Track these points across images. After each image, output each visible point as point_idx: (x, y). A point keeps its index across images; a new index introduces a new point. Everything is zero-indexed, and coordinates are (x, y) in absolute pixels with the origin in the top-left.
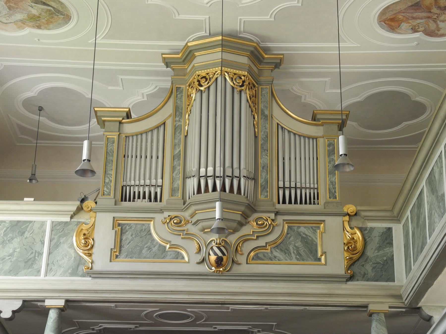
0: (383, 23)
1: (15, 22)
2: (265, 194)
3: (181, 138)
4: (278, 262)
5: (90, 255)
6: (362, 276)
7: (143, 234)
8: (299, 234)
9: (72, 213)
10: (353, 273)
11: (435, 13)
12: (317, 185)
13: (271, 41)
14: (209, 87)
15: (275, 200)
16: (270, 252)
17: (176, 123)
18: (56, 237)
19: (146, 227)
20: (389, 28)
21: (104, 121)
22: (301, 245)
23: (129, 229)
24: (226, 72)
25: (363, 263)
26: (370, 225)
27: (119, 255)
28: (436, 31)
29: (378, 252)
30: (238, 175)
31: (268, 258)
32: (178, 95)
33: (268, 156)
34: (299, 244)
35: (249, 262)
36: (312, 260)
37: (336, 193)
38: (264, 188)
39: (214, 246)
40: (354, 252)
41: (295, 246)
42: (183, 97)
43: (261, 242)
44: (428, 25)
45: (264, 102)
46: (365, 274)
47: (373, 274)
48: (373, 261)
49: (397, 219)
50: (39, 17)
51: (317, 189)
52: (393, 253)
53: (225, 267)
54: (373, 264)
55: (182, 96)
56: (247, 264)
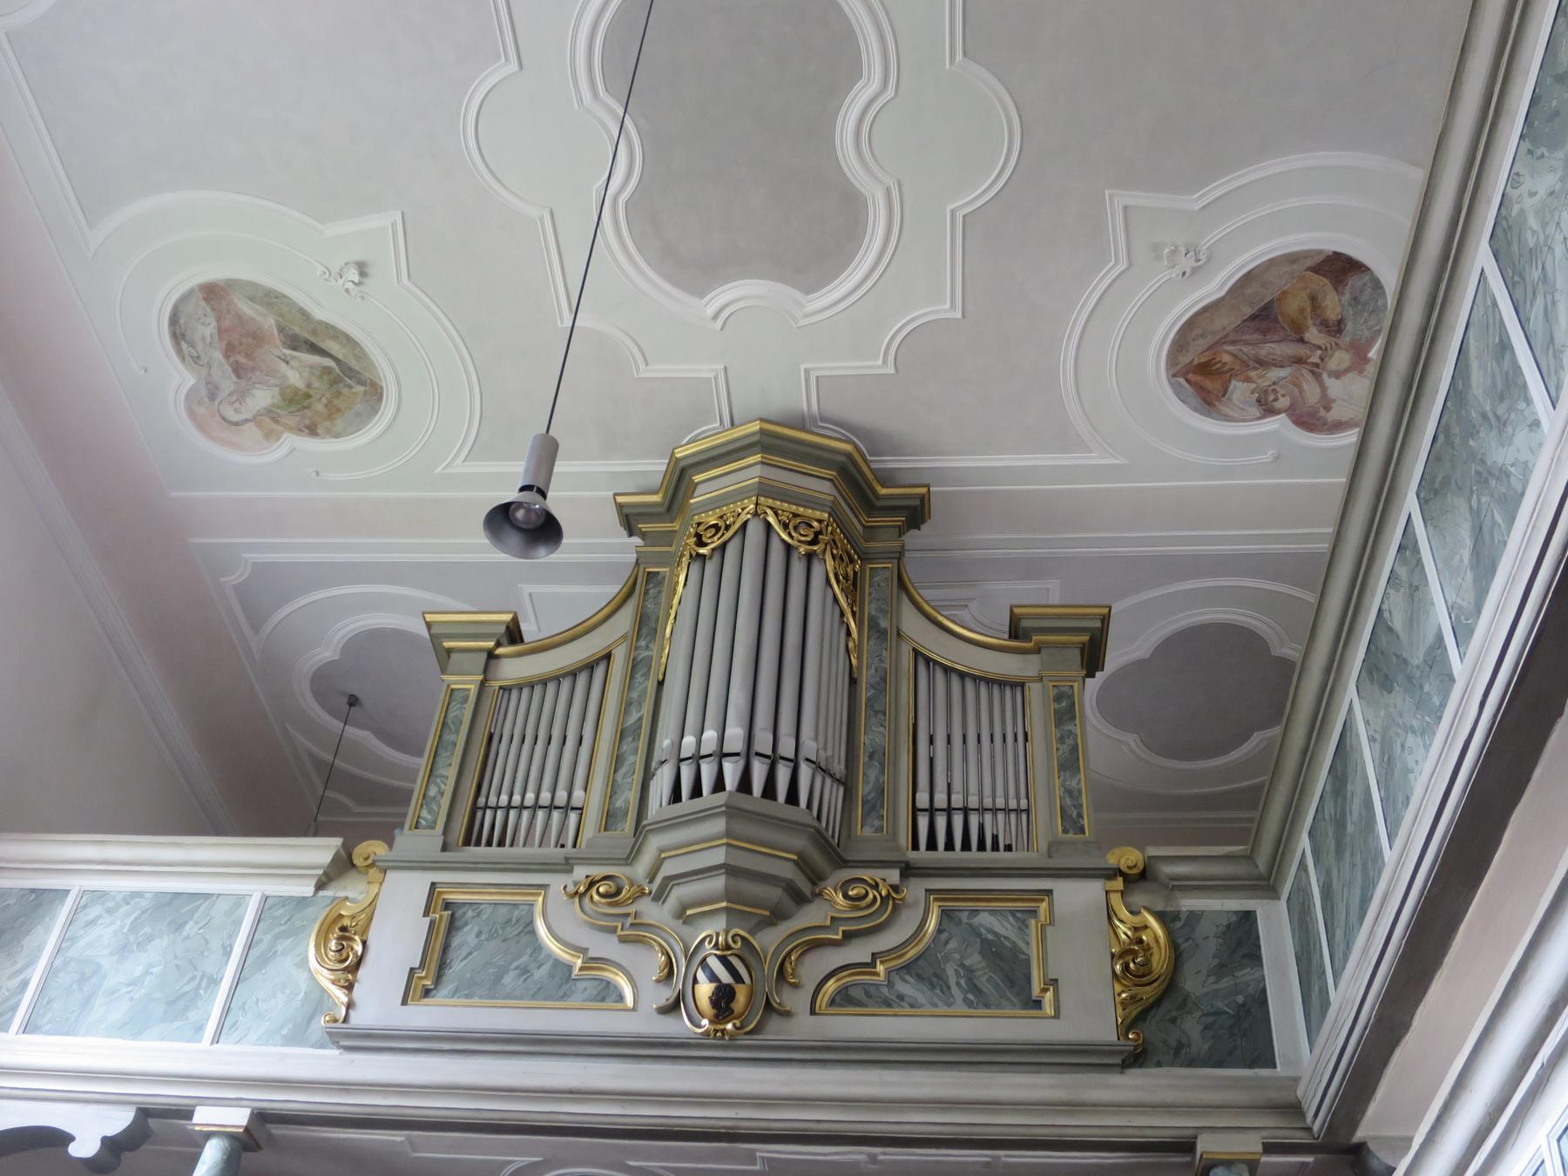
0: (1182, 380)
1: (256, 419)
2: (874, 823)
3: (646, 688)
4: (908, 1010)
5: (349, 987)
6: (1172, 1052)
7: (512, 931)
8: (975, 931)
9: (320, 872)
10: (1143, 1041)
11: (1314, 345)
12: (1026, 801)
13: (897, 450)
14: (723, 547)
15: (904, 838)
16: (886, 983)
17: (636, 653)
18: (267, 938)
19: (523, 913)
20: (1200, 401)
21: (449, 651)
22: (980, 962)
23: (473, 917)
24: (771, 508)
25: (1174, 1014)
26: (1189, 903)
27: (432, 987)
28: (1321, 409)
29: (1216, 982)
30: (791, 755)
31: (877, 999)
32: (651, 592)
33: (885, 727)
34: (975, 960)
35: (820, 1010)
36: (1014, 1006)
37: (1083, 819)
38: (872, 808)
39: (711, 954)
40: (1144, 979)
41: (962, 965)
42: (664, 593)
43: (859, 952)
44: (1301, 391)
45: (878, 600)
46: (1180, 1046)
47: (1206, 1046)
48: (1202, 1007)
49: (1267, 886)
50: (308, 396)
51: (1028, 811)
52: (1265, 985)
53: (741, 1022)
54: (1204, 1015)
55: (660, 592)
56: (811, 1014)
